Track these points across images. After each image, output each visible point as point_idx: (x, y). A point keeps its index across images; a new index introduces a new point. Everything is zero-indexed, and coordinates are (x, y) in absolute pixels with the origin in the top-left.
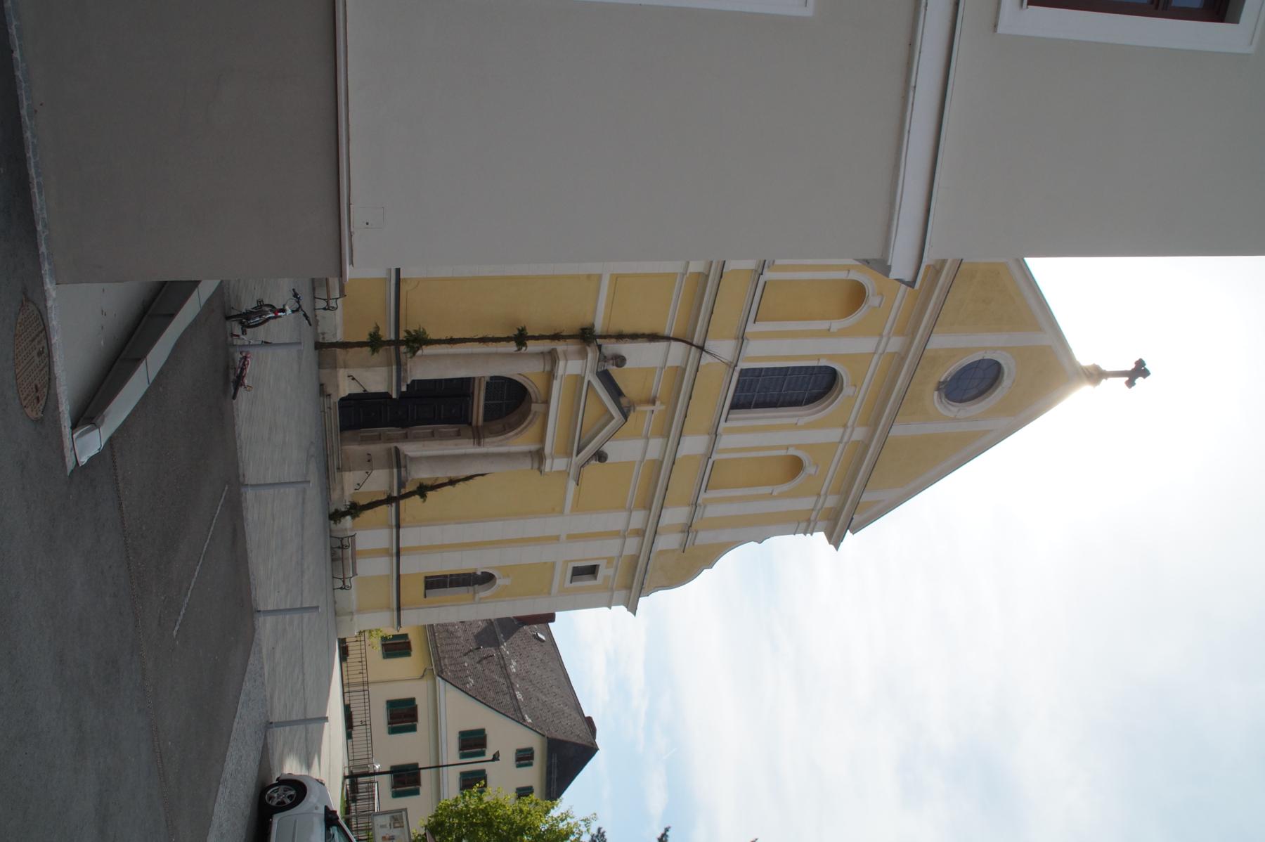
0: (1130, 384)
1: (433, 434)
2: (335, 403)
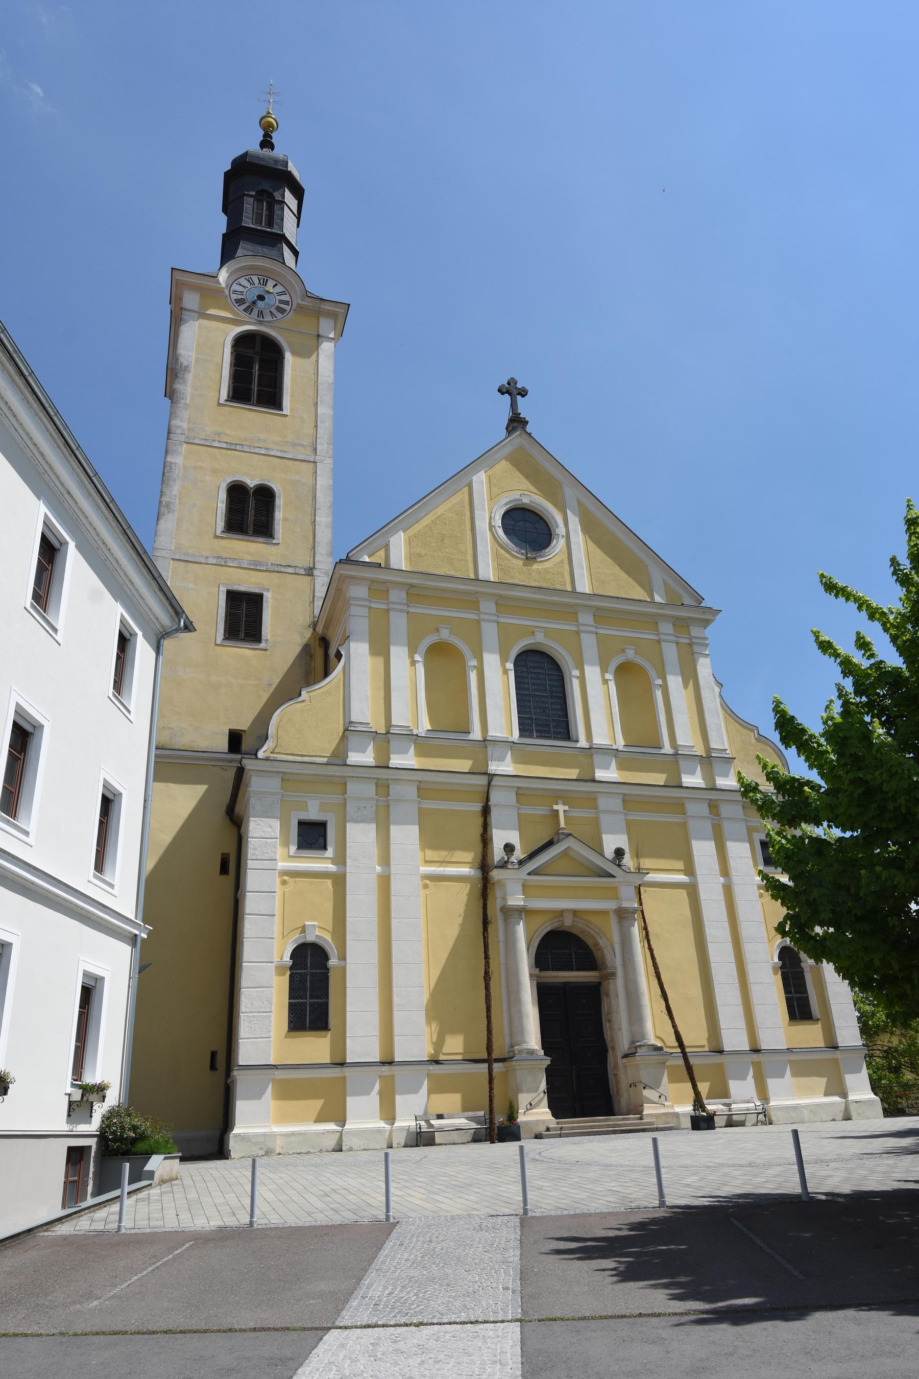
0: (523, 393)
1: (609, 1021)
2: (557, 1122)
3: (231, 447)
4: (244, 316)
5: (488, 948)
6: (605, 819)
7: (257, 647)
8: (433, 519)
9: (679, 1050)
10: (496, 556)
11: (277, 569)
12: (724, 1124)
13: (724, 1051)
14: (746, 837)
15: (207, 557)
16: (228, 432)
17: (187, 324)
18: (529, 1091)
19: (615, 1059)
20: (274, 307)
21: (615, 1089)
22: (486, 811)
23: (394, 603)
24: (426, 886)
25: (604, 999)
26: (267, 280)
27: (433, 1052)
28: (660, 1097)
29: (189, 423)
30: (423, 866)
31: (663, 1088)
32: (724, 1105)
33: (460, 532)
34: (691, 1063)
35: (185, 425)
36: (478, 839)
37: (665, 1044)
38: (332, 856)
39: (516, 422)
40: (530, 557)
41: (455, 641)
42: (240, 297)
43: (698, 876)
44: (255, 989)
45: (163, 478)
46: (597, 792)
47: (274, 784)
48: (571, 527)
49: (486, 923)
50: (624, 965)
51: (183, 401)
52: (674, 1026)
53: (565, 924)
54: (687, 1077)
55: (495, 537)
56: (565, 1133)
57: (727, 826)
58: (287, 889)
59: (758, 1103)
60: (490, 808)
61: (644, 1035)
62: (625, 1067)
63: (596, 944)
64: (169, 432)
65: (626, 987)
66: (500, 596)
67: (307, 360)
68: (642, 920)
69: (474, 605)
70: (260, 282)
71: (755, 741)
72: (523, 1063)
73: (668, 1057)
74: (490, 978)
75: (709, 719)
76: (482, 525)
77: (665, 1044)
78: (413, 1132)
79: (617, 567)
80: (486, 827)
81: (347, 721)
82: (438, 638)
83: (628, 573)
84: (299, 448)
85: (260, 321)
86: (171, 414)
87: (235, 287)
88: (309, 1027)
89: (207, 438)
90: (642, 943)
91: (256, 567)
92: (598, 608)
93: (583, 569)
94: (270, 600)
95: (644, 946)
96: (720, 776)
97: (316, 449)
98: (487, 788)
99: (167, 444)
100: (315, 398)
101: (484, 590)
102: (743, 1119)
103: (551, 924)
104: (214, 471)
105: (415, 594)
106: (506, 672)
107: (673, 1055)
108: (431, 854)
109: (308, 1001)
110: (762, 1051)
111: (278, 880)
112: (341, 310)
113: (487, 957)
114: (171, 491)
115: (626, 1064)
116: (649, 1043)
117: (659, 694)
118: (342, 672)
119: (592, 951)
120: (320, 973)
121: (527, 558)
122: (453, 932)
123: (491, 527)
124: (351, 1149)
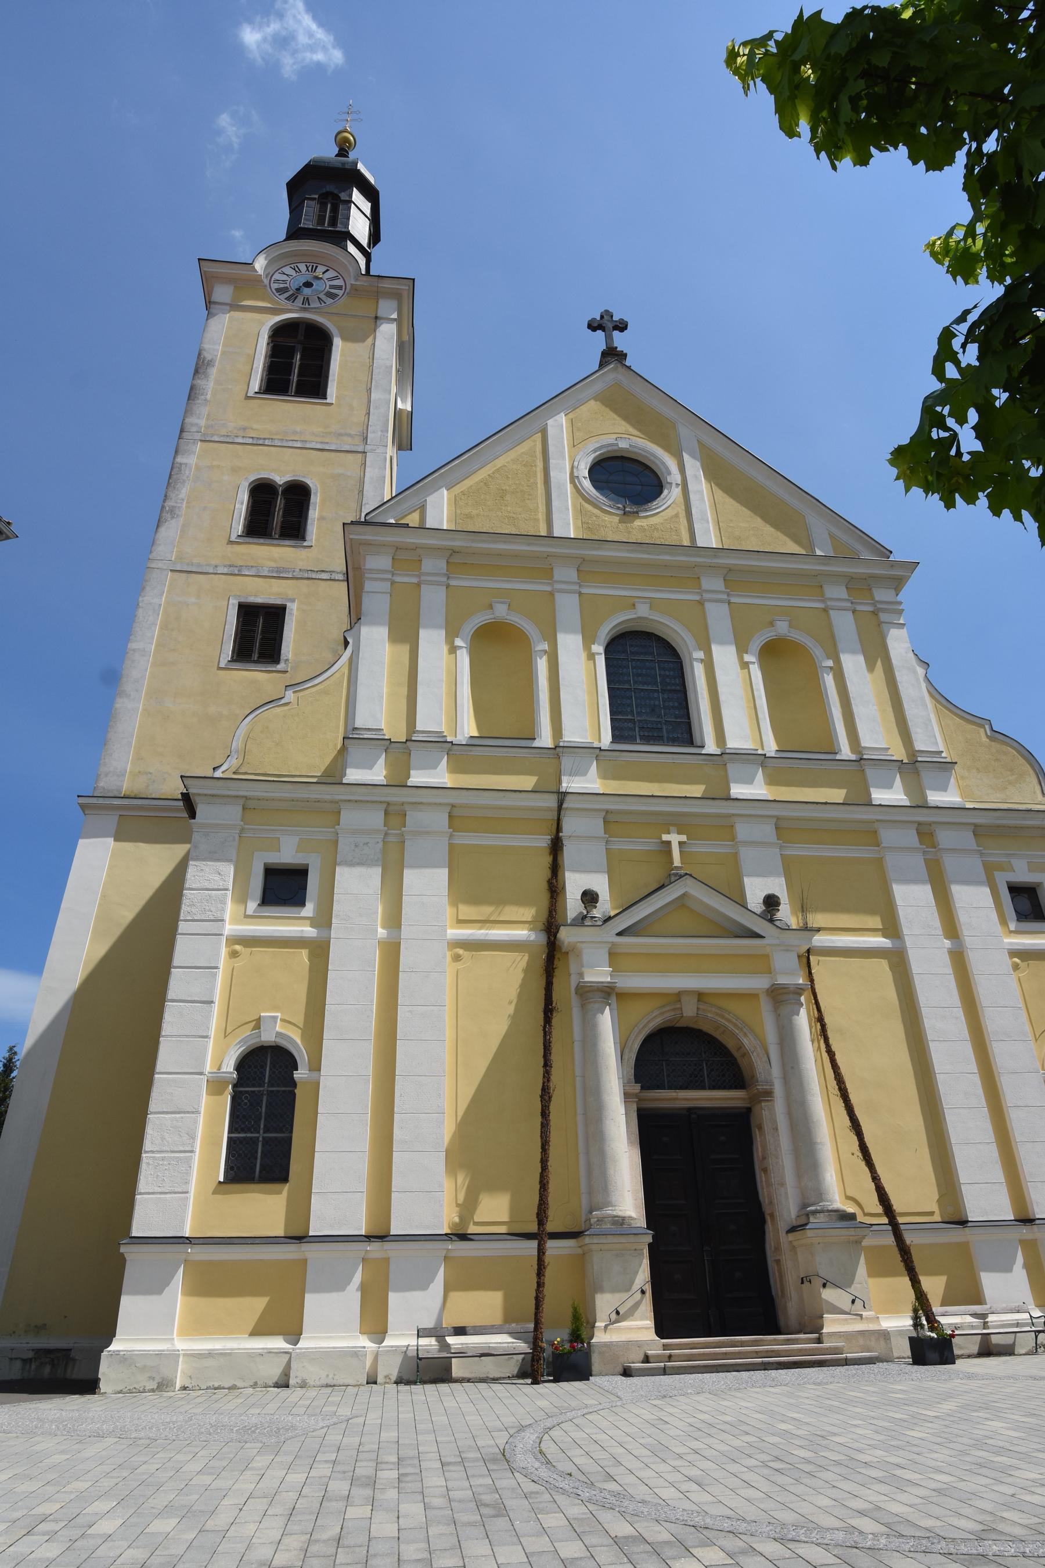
0: (622, 326)
1: (765, 1170)
3: (258, 443)
4: (289, 305)
5: (549, 1050)
6: (747, 855)
7: (274, 669)
9: (885, 1220)
10: (580, 512)
11: (308, 576)
12: (975, 1349)
13: (968, 1221)
14: (983, 877)
15: (216, 566)
16: (255, 426)
17: (215, 318)
18: (615, 1290)
19: (776, 1234)
20: (324, 293)
21: (779, 1286)
22: (556, 846)
23: (428, 574)
24: (457, 958)
25: (756, 1133)
26: (317, 267)
27: (457, 1220)
28: (853, 1302)
29: (207, 419)
30: (452, 927)
31: (858, 1286)
32: (975, 1315)
33: (528, 486)
34: (908, 1242)
35: (202, 423)
36: (543, 886)
37: (863, 1210)
38: (311, 915)
39: (612, 355)
41: (516, 620)
42: (282, 286)
43: (906, 938)
44: (170, 1116)
45: (169, 481)
46: (734, 815)
47: (232, 813)
48: (689, 472)
49: (548, 1011)
50: (785, 1078)
52: (876, 1179)
53: (685, 1015)
54: (901, 1266)
55: (578, 490)
56: (673, 1367)
57: (950, 863)
58: (238, 963)
59: (1037, 1313)
60: (562, 841)
61: (821, 1194)
62: (793, 1248)
63: (740, 1047)
64: (182, 431)
65: (790, 1114)
66: (584, 560)
67: (361, 344)
68: (815, 1006)
69: (548, 573)
70: (308, 270)
71: (988, 740)
72: (603, 1240)
73: (866, 1231)
74: (550, 1098)
75: (911, 711)
76: (560, 476)
77: (863, 1210)
78: (413, 1357)
79: (759, 520)
80: (556, 869)
81: (350, 728)
82: (492, 616)
83: (773, 525)
84: (345, 438)
85: (305, 308)
86: (186, 412)
87: (277, 276)
88: (260, 1177)
89: (229, 434)
90: (816, 1044)
91: (279, 574)
92: (730, 570)
93: (708, 523)
94: (295, 612)
95: (819, 1048)
96: (931, 789)
97: (367, 438)
98: (556, 814)
99: (178, 444)
100: (369, 383)
101: (558, 550)
102: (1011, 1342)
103: (662, 1013)
104: (235, 470)
106: (591, 657)
107: (875, 1228)
108: (467, 911)
109: (261, 1135)
110: (1037, 1222)
111: (224, 951)
112: (404, 287)
113: (547, 1064)
114: (177, 495)
115: (795, 1243)
116: (830, 1208)
117: (829, 680)
118: (347, 664)
119: (735, 1059)
120: (284, 1091)
121: (624, 514)
122: (497, 1027)
123: (573, 478)
124: (303, 1385)
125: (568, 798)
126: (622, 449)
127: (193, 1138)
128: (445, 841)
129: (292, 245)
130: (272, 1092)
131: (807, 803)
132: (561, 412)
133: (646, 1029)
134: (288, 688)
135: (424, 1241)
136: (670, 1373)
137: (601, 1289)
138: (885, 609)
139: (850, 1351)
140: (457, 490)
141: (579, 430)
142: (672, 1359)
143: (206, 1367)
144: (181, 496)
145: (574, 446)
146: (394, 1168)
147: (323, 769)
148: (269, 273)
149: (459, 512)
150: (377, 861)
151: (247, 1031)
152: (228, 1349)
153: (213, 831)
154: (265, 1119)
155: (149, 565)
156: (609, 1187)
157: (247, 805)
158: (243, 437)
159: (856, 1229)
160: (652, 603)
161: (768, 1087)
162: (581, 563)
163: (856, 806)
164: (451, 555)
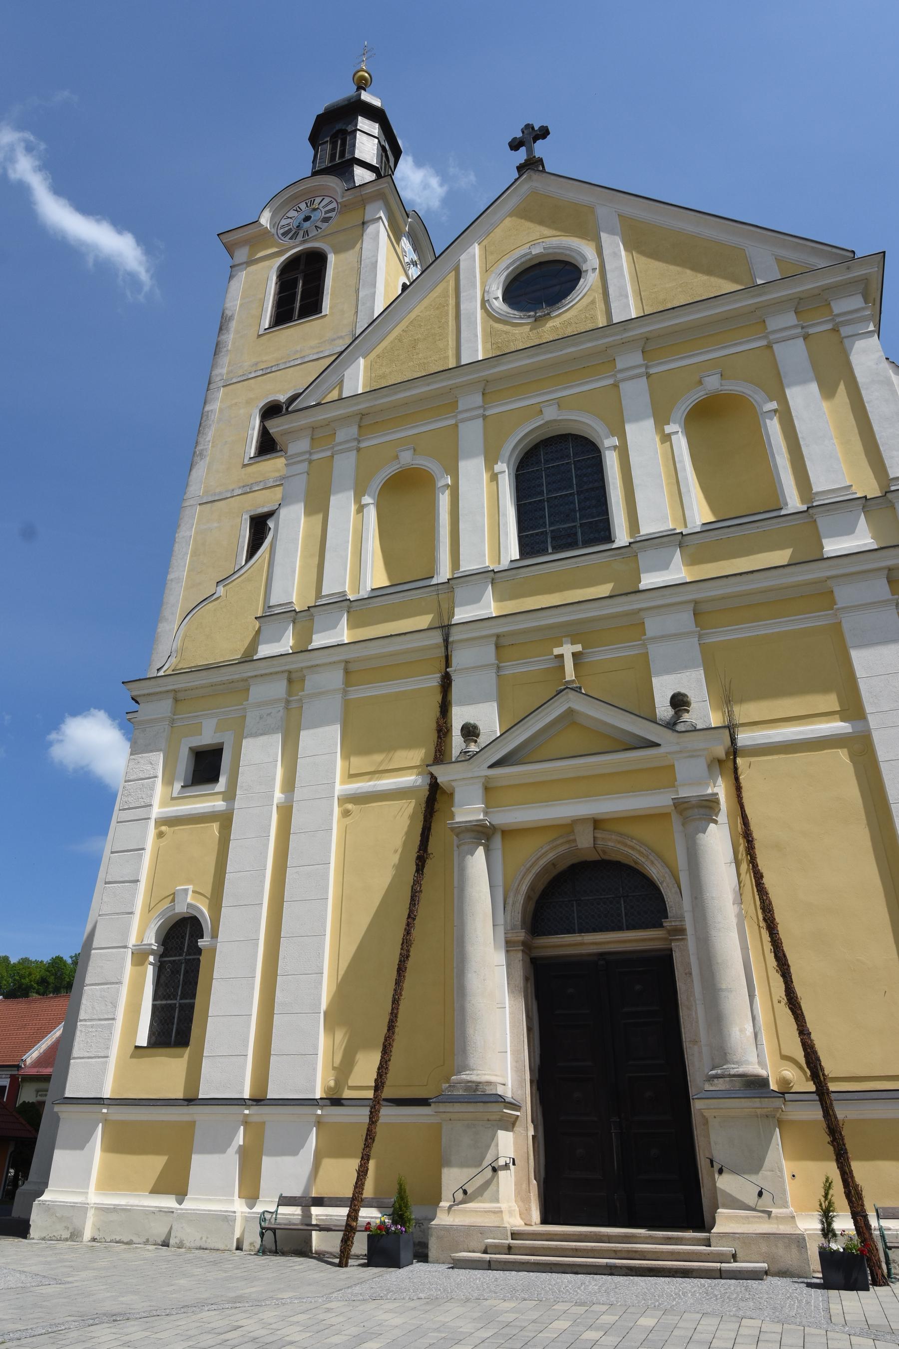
3: (267, 372)
8: (403, 328)
15: (233, 490)
16: (264, 359)
27: (332, 1083)
28: (760, 1194)
31: (769, 1173)
39: (532, 165)
40: (540, 316)
42: (286, 229)
46: (641, 610)
47: (164, 707)
51: (225, 349)
52: (803, 1032)
58: (164, 842)
61: (725, 1054)
64: (209, 384)
79: (688, 272)
80: (445, 708)
82: (398, 466)
87: (284, 222)
88: (175, 1042)
98: (443, 649)
103: (552, 849)
105: (370, 424)
108: (360, 763)
111: (152, 832)
116: (733, 1072)
125: (454, 630)
126: (537, 256)
127: (115, 1006)
128: (339, 697)
129: (290, 190)
130: (189, 960)
131: (741, 574)
132: (474, 243)
133: (536, 868)
134: (219, 584)
135: (293, 1105)
136: (496, 1268)
137: (449, 1164)
138: (847, 320)
139: (747, 1259)
140: (373, 355)
141: (492, 253)
142: (513, 1251)
143: (111, 1221)
144: (207, 439)
145: (487, 271)
146: (274, 1030)
147: (243, 650)
148: (276, 222)
149: (373, 375)
150: (277, 728)
151: (166, 904)
152: (129, 1206)
153: (148, 726)
154: (183, 987)
155: (183, 506)
156: (469, 1048)
157: (177, 697)
158: (255, 371)
159: (762, 1099)
160: (559, 403)
161: (677, 923)
162: (486, 385)
163: (794, 566)
164: (361, 419)
